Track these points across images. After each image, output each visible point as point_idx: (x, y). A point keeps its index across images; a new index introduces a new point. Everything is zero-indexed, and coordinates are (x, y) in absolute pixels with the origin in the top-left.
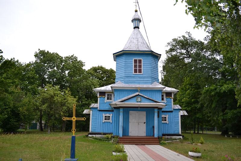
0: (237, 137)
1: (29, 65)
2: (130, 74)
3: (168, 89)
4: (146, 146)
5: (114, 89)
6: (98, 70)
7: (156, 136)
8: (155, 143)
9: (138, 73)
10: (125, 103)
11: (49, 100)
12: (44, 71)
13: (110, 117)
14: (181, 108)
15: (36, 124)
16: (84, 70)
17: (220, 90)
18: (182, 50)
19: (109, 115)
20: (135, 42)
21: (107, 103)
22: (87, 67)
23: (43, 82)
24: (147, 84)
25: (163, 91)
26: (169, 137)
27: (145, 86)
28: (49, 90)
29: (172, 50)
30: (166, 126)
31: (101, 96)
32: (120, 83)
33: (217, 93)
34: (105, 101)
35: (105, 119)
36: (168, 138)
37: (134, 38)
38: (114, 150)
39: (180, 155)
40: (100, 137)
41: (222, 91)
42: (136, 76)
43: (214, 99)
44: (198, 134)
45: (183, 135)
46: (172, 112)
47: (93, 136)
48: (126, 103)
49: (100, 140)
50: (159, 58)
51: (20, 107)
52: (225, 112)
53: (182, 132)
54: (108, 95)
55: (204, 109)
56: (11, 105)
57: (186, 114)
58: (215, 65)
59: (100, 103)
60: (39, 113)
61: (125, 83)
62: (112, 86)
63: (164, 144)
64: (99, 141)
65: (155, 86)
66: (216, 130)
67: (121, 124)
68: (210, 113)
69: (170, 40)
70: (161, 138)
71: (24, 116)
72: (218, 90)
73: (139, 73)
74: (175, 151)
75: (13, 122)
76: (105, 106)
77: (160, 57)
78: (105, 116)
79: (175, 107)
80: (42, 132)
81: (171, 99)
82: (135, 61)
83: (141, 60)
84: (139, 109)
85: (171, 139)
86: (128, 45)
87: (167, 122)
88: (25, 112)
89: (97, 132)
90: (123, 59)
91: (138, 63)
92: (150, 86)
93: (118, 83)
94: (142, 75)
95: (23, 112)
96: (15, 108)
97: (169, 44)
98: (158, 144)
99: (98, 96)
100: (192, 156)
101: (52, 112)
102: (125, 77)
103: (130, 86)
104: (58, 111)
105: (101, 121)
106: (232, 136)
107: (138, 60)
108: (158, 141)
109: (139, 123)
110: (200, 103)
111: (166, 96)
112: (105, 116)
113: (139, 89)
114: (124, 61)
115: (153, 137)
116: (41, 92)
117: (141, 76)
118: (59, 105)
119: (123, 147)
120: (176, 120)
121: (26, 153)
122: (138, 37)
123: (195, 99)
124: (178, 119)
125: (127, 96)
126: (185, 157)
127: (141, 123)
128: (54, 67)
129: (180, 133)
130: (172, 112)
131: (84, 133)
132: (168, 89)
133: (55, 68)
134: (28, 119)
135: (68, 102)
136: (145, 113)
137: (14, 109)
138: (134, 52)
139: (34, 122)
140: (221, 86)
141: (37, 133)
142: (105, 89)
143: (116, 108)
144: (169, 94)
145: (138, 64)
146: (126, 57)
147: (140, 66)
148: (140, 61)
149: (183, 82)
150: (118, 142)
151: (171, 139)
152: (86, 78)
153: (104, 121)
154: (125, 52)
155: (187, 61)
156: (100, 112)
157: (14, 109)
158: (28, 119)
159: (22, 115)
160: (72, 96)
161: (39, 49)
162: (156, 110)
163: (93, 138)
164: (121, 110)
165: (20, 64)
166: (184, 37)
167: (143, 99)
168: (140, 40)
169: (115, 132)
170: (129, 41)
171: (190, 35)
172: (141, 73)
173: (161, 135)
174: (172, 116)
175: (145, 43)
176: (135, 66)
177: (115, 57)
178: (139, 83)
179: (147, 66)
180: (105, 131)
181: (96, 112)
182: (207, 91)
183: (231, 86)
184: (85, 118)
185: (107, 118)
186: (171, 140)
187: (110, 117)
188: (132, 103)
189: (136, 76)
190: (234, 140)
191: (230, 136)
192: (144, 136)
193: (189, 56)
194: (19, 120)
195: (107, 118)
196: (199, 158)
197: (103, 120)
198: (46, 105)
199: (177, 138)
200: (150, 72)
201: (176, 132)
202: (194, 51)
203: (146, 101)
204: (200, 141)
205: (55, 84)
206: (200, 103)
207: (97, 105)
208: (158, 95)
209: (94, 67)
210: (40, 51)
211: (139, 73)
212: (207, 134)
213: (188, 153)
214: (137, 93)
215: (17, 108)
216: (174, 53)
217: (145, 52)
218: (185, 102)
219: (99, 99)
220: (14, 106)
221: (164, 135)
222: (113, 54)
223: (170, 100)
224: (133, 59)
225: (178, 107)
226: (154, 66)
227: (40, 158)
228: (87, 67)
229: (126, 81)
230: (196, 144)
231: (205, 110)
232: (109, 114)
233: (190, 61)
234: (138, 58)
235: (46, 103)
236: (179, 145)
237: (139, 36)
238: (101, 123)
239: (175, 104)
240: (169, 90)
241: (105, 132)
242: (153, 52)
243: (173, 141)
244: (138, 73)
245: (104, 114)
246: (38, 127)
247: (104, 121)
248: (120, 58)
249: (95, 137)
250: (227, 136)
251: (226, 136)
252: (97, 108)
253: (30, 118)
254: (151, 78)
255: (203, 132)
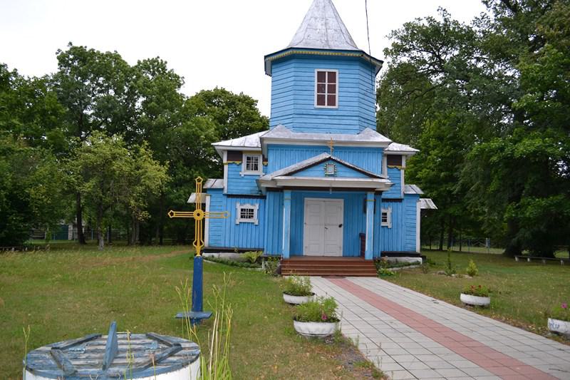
0: (544, 261)
1: (40, 83)
2: (307, 107)
3: (396, 147)
4: (348, 278)
5: (268, 145)
6: (216, 98)
7: (369, 255)
8: (369, 272)
9: (326, 106)
10: (297, 178)
11: (101, 170)
12: (83, 98)
13: (252, 210)
14: (422, 193)
15: (66, 228)
16: (182, 95)
17: (513, 151)
18: (424, 53)
19: (251, 207)
20: (319, 26)
21: (246, 177)
22: (188, 90)
23: (82, 125)
24: (347, 133)
25: (385, 153)
26: (392, 259)
27: (343, 137)
28: (98, 144)
29: (398, 49)
30: (386, 234)
31: (231, 162)
32: (282, 129)
33: (506, 158)
34: (242, 174)
35: (242, 217)
36: (389, 262)
37: (316, 18)
38: (285, 290)
39: (438, 301)
40: (230, 258)
41: (517, 155)
42: (323, 112)
43: (496, 172)
44: (439, 252)
45: (424, 254)
46: (400, 200)
47: (213, 256)
48: (299, 177)
49: (232, 265)
50: (377, 69)
51: (31, 186)
52: (520, 204)
53: (423, 247)
54: (248, 159)
55: (468, 195)
56: (8, 183)
57: (433, 206)
58: (497, 95)
59: (228, 178)
60: (75, 202)
61: (297, 128)
62: (264, 136)
63: (387, 274)
64: (231, 267)
65: (368, 139)
66: (487, 245)
67: (286, 227)
68: (483, 204)
69: (399, 26)
70: (379, 261)
71: (41, 208)
72: (508, 151)
73: (328, 105)
74: (422, 292)
75: (16, 223)
76: (242, 184)
77: (381, 67)
78: (242, 210)
79: (409, 191)
80: (85, 246)
81: (400, 170)
82: (321, 76)
83: (335, 73)
84: (331, 192)
85: (397, 264)
86: (301, 35)
87: (388, 224)
88: (42, 200)
89: (223, 246)
90: (289, 72)
91: (327, 81)
92: (322, 136)
93: (278, 130)
94: (337, 110)
95: (39, 200)
96: (16, 189)
97: (395, 33)
98: (378, 276)
99: (225, 161)
100: (470, 305)
101: (107, 200)
102: (296, 116)
103: (308, 138)
104: (122, 198)
105: (233, 220)
106: (532, 259)
107: (327, 73)
108: (375, 268)
109: (329, 225)
110: (461, 182)
111: (388, 164)
112: (242, 210)
113: (330, 146)
115: (362, 260)
116: (81, 151)
117: (335, 113)
118: (124, 182)
119: (308, 282)
120: (409, 221)
121: (69, 298)
122: (327, 16)
123: (446, 171)
124: (413, 217)
125: (298, 162)
126: (451, 306)
127: (333, 225)
128: (108, 87)
129: (418, 250)
130: (400, 200)
131: (184, 248)
132: (396, 147)
133: (112, 92)
134: (51, 214)
135: (147, 174)
136: (341, 202)
137: (15, 192)
138: (319, 53)
139: (63, 222)
140: (515, 142)
141: (75, 249)
142: (242, 145)
143: (270, 191)
144: (394, 159)
145: (327, 83)
146: (297, 65)
147: (332, 89)
148: (332, 76)
149: (421, 131)
150: (280, 272)
151: (397, 264)
152: (185, 115)
153: (239, 220)
154: (295, 51)
155: (436, 79)
156: (230, 199)
157: (15, 192)
158: (51, 214)
159: (36, 207)
160: (154, 160)
161: (71, 44)
162: (371, 197)
163: (215, 261)
164: (287, 195)
165: (21, 81)
166: (430, 19)
167: (340, 169)
168: (332, 23)
169: (270, 247)
170: (305, 25)
171: (448, 16)
172: (335, 105)
173: (378, 254)
174: (400, 211)
175: (344, 31)
176: (321, 88)
177: (269, 65)
178: (329, 131)
179: (350, 90)
181: (219, 199)
182: (482, 151)
183: (538, 142)
184: (169, 214)
185: (247, 214)
186: (400, 267)
187: (252, 210)
188: (315, 178)
189: (323, 112)
190: (539, 267)
191: (526, 259)
192: (340, 257)
193: (440, 66)
194: (29, 217)
195: (247, 214)
196: (486, 308)
197: (236, 218)
198: (92, 182)
199: (410, 262)
200: (356, 104)
201: (408, 249)
202: (452, 53)
203: (348, 175)
204: (467, 270)
205: (111, 131)
206: (461, 182)
207: (222, 183)
208: (374, 161)
209: (206, 90)
210: (71, 47)
211: (328, 105)
212: (469, 253)
213: (459, 297)
214: (325, 156)
215: (21, 189)
216: (404, 59)
217: (346, 54)
218: (425, 178)
219: (226, 167)
220: (14, 185)
221: (383, 254)
222: (266, 57)
223: (397, 172)
224: (316, 71)
225: (415, 189)
226: (365, 88)
227: (110, 312)
228: (188, 90)
229: (298, 125)
230: (459, 277)
231: (469, 199)
232: (252, 205)
233: (440, 82)
234: (326, 69)
235: (92, 177)
236: (422, 278)
237: (330, 13)
238: (233, 225)
239: (408, 183)
240: (395, 149)
241: (241, 247)
242: (364, 55)
243: (404, 268)
244: (326, 106)
245: (238, 205)
246: (70, 235)
247: (239, 220)
248: (284, 68)
249: (219, 258)
250: (520, 258)
251: (516, 259)
252: (222, 189)
253: (55, 212)
254: (357, 118)
255: (460, 249)
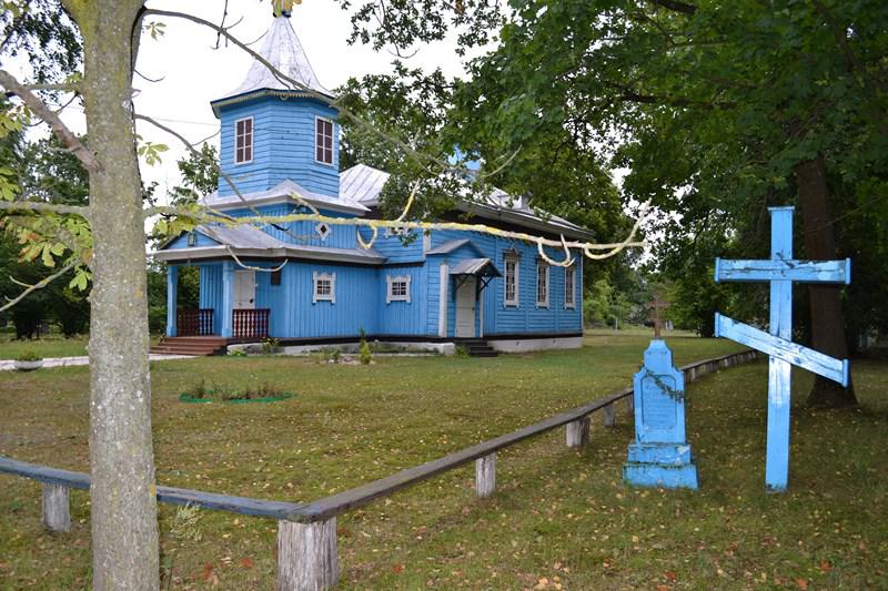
42: (243, 169)
46: (420, 264)
87: (407, 298)
103: (227, 202)
114: (269, 119)
124: (436, 286)
130: (420, 264)
180: (303, 331)
188: (504, 234)
189: (243, 169)
195: (323, 287)
201: (430, 332)
245: (315, 274)
247: (316, 297)
